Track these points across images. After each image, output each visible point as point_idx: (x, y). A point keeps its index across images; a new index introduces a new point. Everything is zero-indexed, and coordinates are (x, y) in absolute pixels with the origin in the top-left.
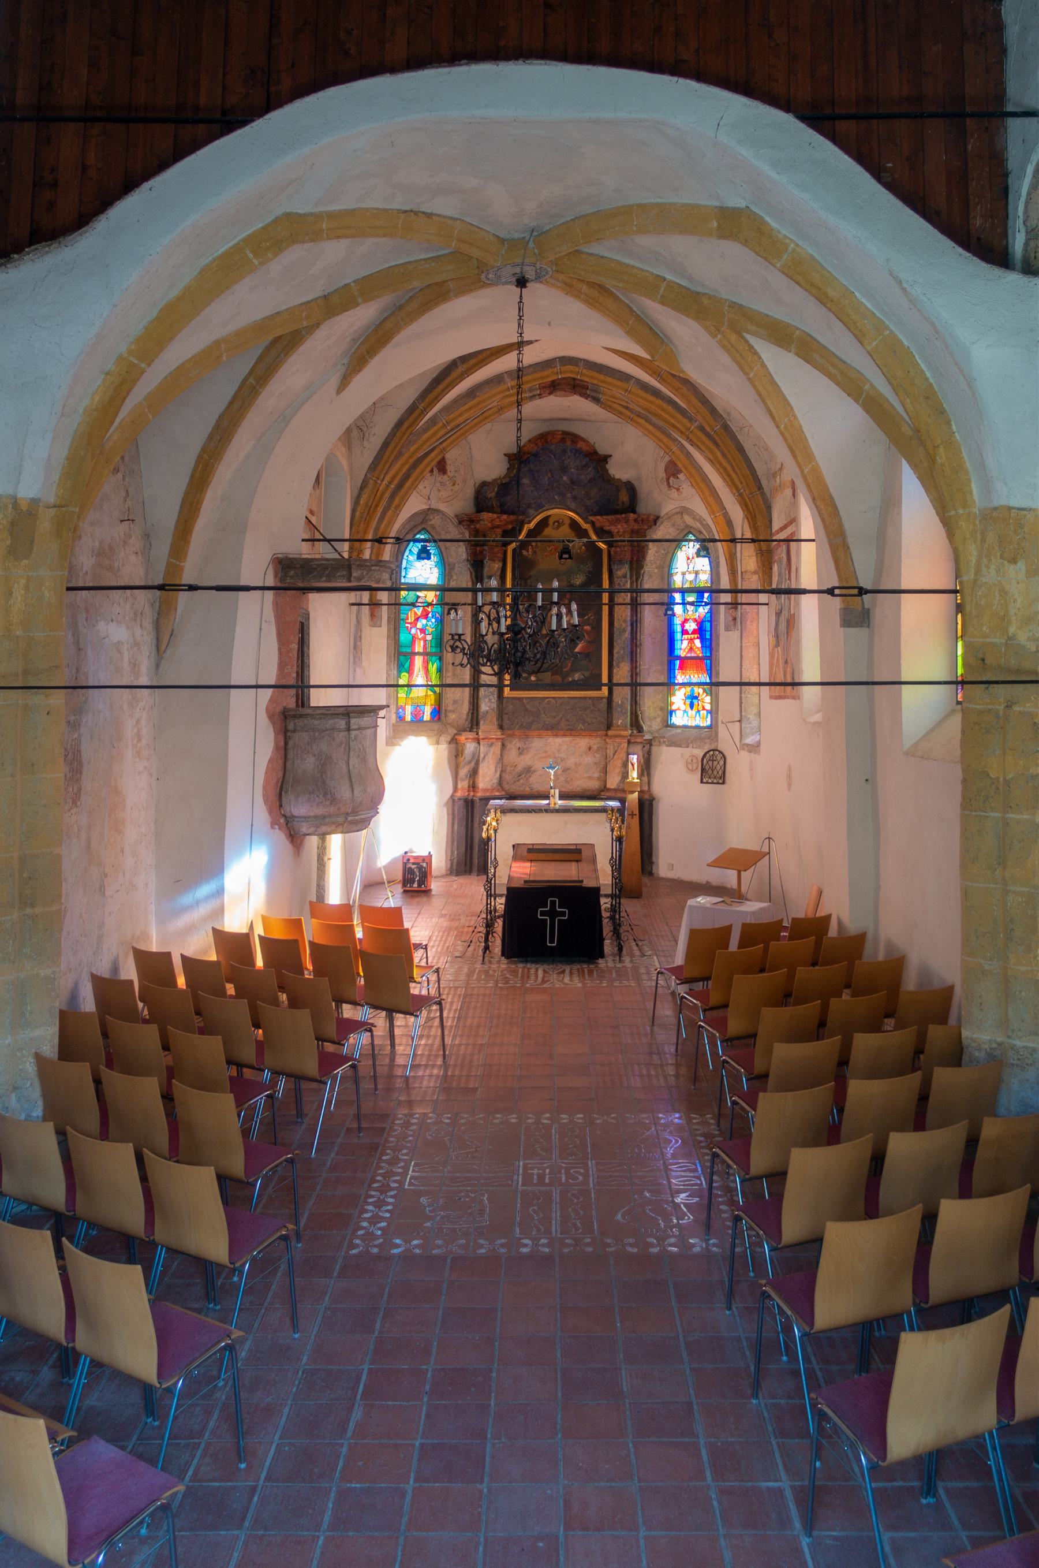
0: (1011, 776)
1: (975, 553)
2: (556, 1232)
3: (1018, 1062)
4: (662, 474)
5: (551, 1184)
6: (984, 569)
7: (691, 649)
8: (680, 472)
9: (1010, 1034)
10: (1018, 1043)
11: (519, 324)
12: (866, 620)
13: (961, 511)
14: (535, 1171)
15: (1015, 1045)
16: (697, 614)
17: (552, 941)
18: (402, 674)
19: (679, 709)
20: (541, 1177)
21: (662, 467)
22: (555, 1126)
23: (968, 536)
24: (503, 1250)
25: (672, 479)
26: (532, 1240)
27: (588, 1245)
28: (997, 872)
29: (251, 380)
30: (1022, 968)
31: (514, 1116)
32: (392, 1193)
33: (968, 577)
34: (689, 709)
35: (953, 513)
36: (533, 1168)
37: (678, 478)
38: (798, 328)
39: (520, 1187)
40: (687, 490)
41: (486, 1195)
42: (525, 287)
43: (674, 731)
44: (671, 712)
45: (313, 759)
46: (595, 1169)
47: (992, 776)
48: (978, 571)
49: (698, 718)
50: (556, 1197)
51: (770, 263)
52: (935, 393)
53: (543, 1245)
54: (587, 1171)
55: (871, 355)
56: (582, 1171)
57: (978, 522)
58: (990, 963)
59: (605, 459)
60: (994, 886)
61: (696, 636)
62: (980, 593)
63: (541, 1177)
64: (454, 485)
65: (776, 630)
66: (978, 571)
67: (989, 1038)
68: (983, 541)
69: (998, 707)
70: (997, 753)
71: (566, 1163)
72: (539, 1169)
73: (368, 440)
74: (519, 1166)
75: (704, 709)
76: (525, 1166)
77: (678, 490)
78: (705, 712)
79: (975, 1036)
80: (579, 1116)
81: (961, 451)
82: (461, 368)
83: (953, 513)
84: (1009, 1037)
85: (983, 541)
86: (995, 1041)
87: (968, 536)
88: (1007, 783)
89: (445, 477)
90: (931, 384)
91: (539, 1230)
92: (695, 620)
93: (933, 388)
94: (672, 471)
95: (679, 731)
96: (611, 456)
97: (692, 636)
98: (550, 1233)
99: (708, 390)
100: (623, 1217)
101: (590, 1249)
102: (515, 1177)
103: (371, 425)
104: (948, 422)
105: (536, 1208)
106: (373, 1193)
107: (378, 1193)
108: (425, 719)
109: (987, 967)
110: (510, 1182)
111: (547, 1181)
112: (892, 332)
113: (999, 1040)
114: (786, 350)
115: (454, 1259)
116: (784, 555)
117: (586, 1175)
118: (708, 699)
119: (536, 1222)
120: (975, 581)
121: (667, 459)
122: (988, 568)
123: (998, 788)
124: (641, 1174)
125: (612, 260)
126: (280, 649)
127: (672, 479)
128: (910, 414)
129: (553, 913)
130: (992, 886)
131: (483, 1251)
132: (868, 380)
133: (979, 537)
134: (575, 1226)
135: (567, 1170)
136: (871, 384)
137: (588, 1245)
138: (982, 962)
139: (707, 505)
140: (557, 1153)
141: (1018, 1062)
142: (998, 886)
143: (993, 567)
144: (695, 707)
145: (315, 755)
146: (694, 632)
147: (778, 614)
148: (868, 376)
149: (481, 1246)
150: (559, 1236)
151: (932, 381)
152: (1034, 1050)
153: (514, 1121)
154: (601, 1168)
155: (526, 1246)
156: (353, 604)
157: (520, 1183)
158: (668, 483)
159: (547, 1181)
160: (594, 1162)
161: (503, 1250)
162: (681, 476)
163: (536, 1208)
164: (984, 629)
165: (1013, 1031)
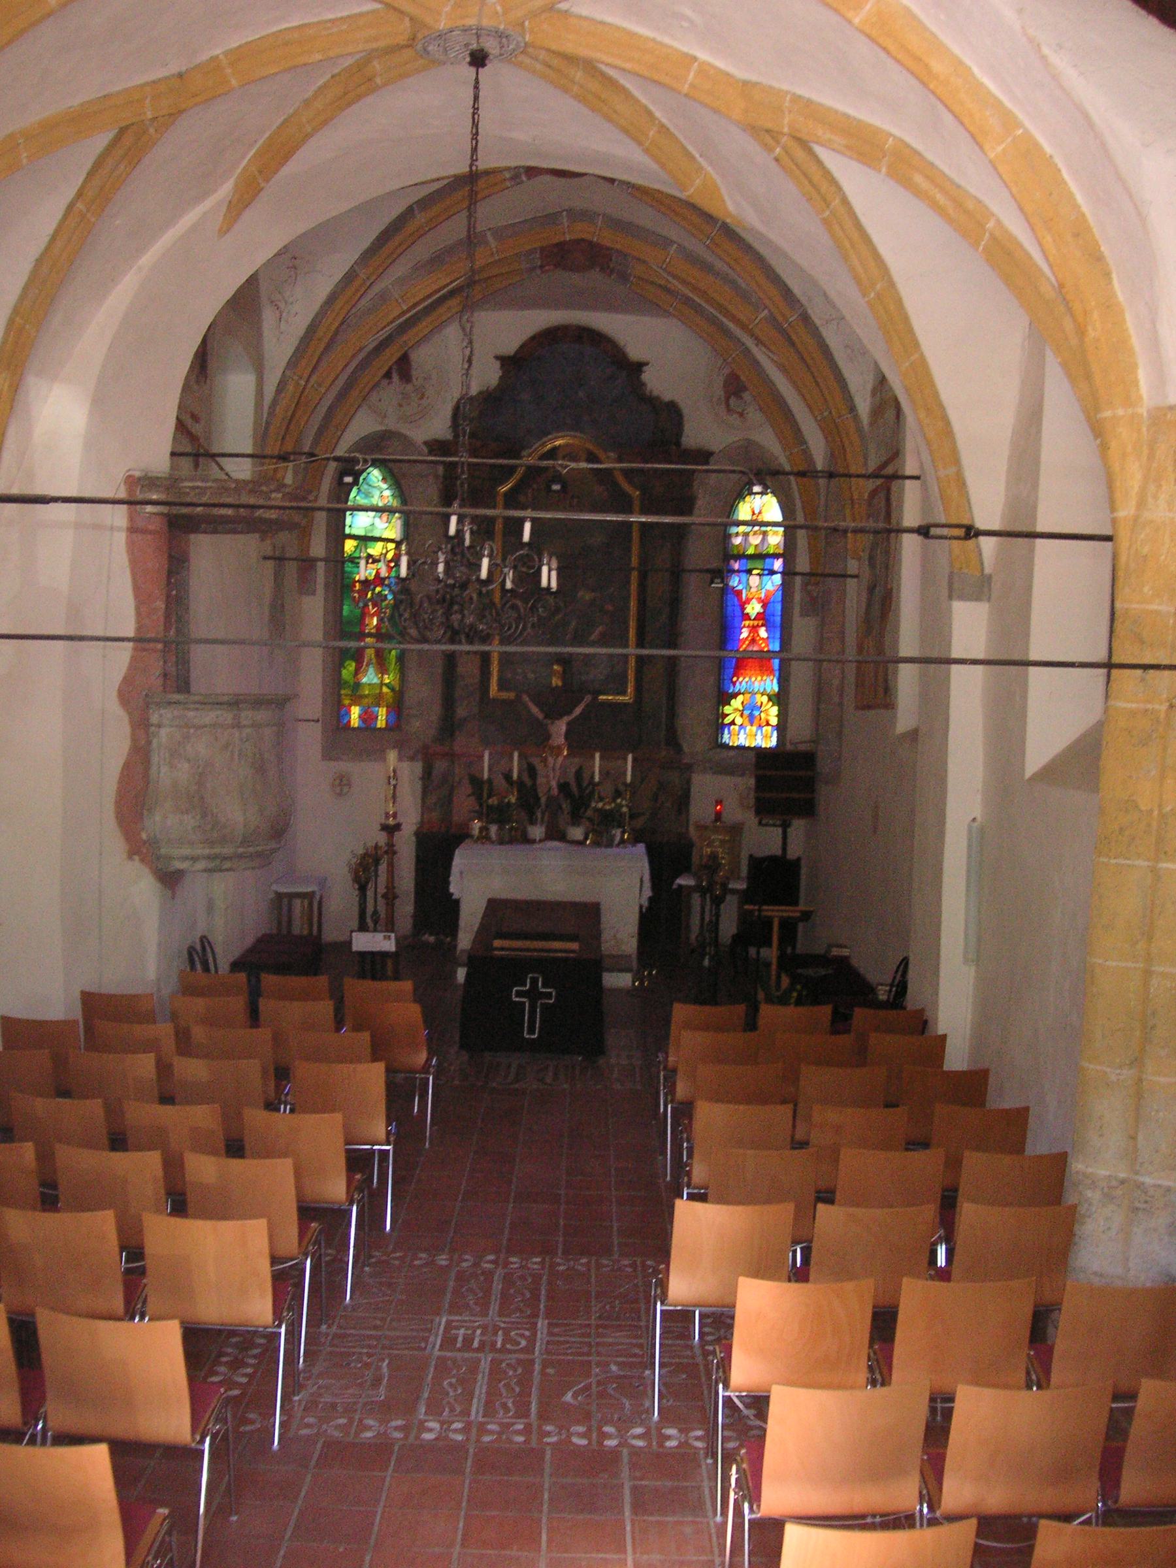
0: (1168, 809)
1: (1138, 476)
2: (477, 1413)
3: (1145, 1206)
4: (720, 392)
5: (481, 1348)
6: (1150, 500)
7: (753, 641)
8: (745, 389)
9: (1138, 1168)
10: (1148, 1180)
11: (477, 129)
12: (986, 590)
13: (1120, 412)
14: (462, 1331)
15: (1143, 1184)
16: (764, 591)
17: (531, 1031)
18: (347, 663)
19: (733, 723)
20: (468, 1341)
21: (719, 382)
22: (500, 1272)
23: (1129, 449)
24: (398, 1435)
25: (732, 401)
26: (442, 1423)
27: (518, 1432)
28: (1138, 947)
29: (80, 206)
30: (1162, 1080)
31: (444, 1257)
32: (256, 1351)
33: (1125, 512)
34: (747, 722)
35: (1108, 414)
36: (458, 1328)
37: (742, 398)
38: (891, 135)
39: (436, 1353)
40: (754, 415)
41: (387, 1362)
42: (483, 65)
43: (725, 754)
44: (723, 726)
45: (186, 765)
46: (545, 1331)
47: (1143, 808)
48: (1141, 504)
49: (759, 737)
50: (485, 1366)
51: (843, 16)
52: (1088, 229)
53: (455, 1431)
54: (535, 1334)
55: (995, 168)
56: (527, 1333)
57: (1144, 429)
58: (1118, 1071)
59: (639, 366)
60: (1133, 965)
61: (760, 623)
62: (1142, 536)
63: (468, 1341)
64: (421, 398)
65: (867, 612)
66: (1141, 504)
67: (1108, 1173)
68: (1151, 456)
69: (1157, 707)
70: (1153, 773)
71: (504, 1322)
72: (467, 1328)
73: (287, 322)
74: (440, 1324)
75: (768, 724)
76: (448, 1323)
77: (741, 415)
78: (770, 728)
79: (1090, 1170)
80: (535, 1260)
81: (1124, 321)
82: (421, 218)
83: (1108, 414)
84: (1137, 1173)
85: (1151, 456)
86: (1116, 1178)
87: (1129, 449)
88: (1163, 816)
89: (409, 387)
90: (1083, 215)
91: (452, 1410)
92: (760, 600)
93: (1086, 221)
94: (734, 388)
95: (732, 753)
96: (647, 364)
97: (756, 623)
98: (469, 1415)
99: (769, 243)
100: (575, 1396)
101: (520, 1439)
102: (431, 1339)
103: (291, 300)
104: (1107, 275)
105: (454, 1380)
106: (229, 1350)
107: (236, 1351)
108: (379, 725)
109: (1113, 1078)
110: (423, 1345)
111: (476, 1344)
112: (1026, 131)
113: (1122, 1175)
114: (874, 169)
115: (328, 1445)
116: (883, 504)
117: (532, 1341)
118: (775, 710)
119: (452, 1400)
120: (1136, 519)
121: (726, 371)
122: (1155, 497)
123: (1149, 825)
124: (610, 1340)
125: (618, 28)
126: (137, 609)
127: (732, 401)
128: (1051, 259)
129: (533, 994)
130: (1130, 965)
131: (369, 1434)
132: (993, 215)
133: (1146, 451)
134: (504, 1406)
135: (506, 1332)
136: (998, 222)
137: (518, 1432)
138: (1108, 1070)
139: (780, 436)
140: (497, 1308)
141: (1145, 1206)
142: (1137, 965)
143: (1162, 497)
144: (756, 721)
145: (189, 761)
146: (759, 616)
147: (871, 589)
148: (995, 208)
149: (369, 1428)
150: (481, 1419)
151: (1085, 209)
152: (1169, 1189)
153: (444, 1263)
154: (556, 1330)
155: (431, 1430)
156: (265, 558)
157: (437, 1347)
158: (728, 405)
159: (476, 1344)
160: (547, 1321)
161: (398, 1435)
162: (746, 396)
163: (454, 1380)
164: (1146, 589)
165: (1142, 1164)
